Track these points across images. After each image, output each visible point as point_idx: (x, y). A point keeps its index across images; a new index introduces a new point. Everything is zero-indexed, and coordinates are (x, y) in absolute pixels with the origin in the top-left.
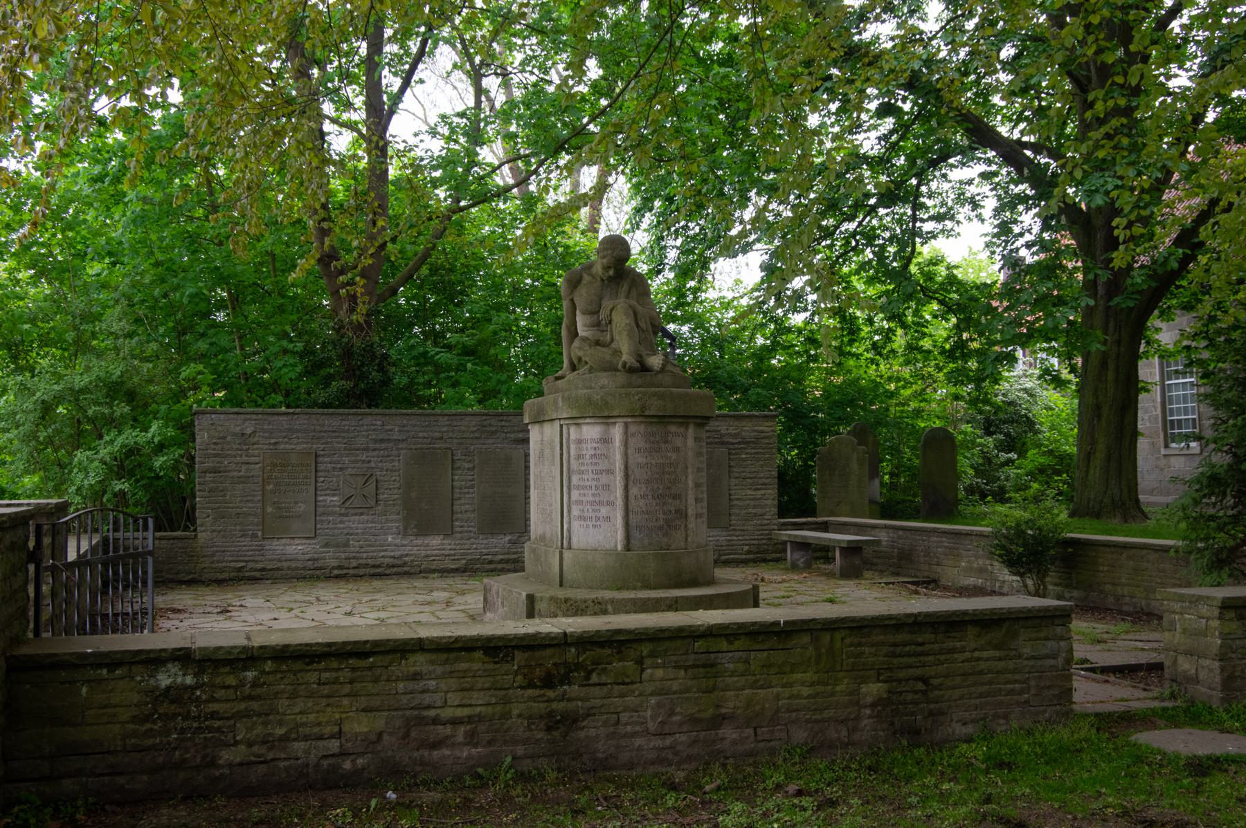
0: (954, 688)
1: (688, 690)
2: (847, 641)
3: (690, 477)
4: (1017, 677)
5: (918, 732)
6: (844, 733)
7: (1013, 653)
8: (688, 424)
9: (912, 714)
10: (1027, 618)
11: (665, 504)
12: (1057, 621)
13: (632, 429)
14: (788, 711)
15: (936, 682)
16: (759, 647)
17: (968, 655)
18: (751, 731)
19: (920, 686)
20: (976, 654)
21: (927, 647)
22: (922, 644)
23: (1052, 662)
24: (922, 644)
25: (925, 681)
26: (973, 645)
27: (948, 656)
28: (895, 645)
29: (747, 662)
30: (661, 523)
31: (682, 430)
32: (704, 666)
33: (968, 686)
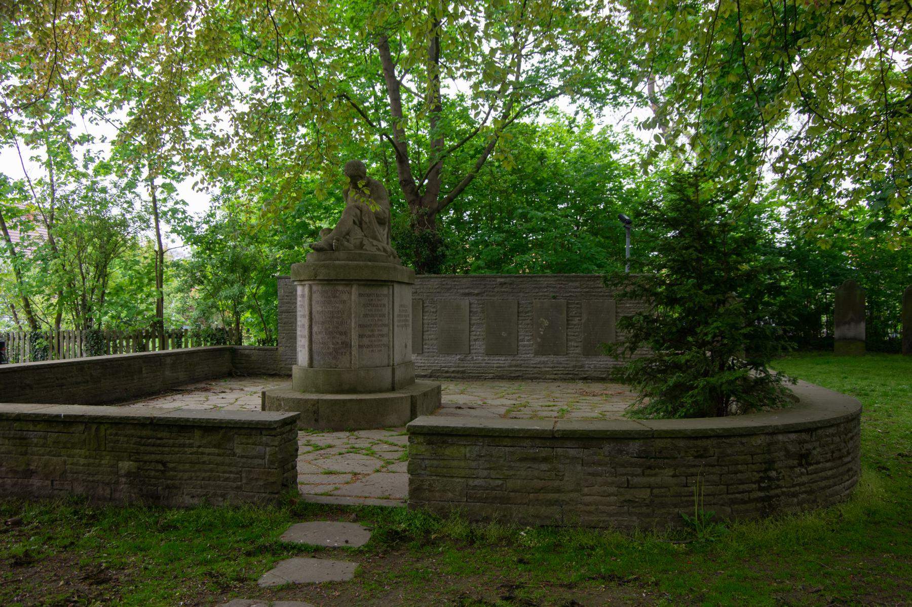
0: (184, 471)
1: (10, 452)
2: (108, 432)
3: (353, 321)
4: (233, 469)
5: (158, 498)
6: (108, 491)
7: (228, 452)
8: (352, 285)
9: (155, 485)
10: (240, 428)
11: (334, 338)
12: (264, 432)
13: (315, 288)
14: (71, 472)
15: (171, 465)
16: (52, 430)
17: (195, 449)
18: (49, 482)
19: (160, 467)
20: (200, 450)
21: (165, 441)
22: (161, 439)
23: (260, 461)
24: (161, 439)
25: (164, 464)
26: (197, 443)
27: (181, 449)
28: (142, 438)
29: (45, 438)
30: (331, 350)
31: (348, 289)
32: (20, 438)
33: (195, 471)
